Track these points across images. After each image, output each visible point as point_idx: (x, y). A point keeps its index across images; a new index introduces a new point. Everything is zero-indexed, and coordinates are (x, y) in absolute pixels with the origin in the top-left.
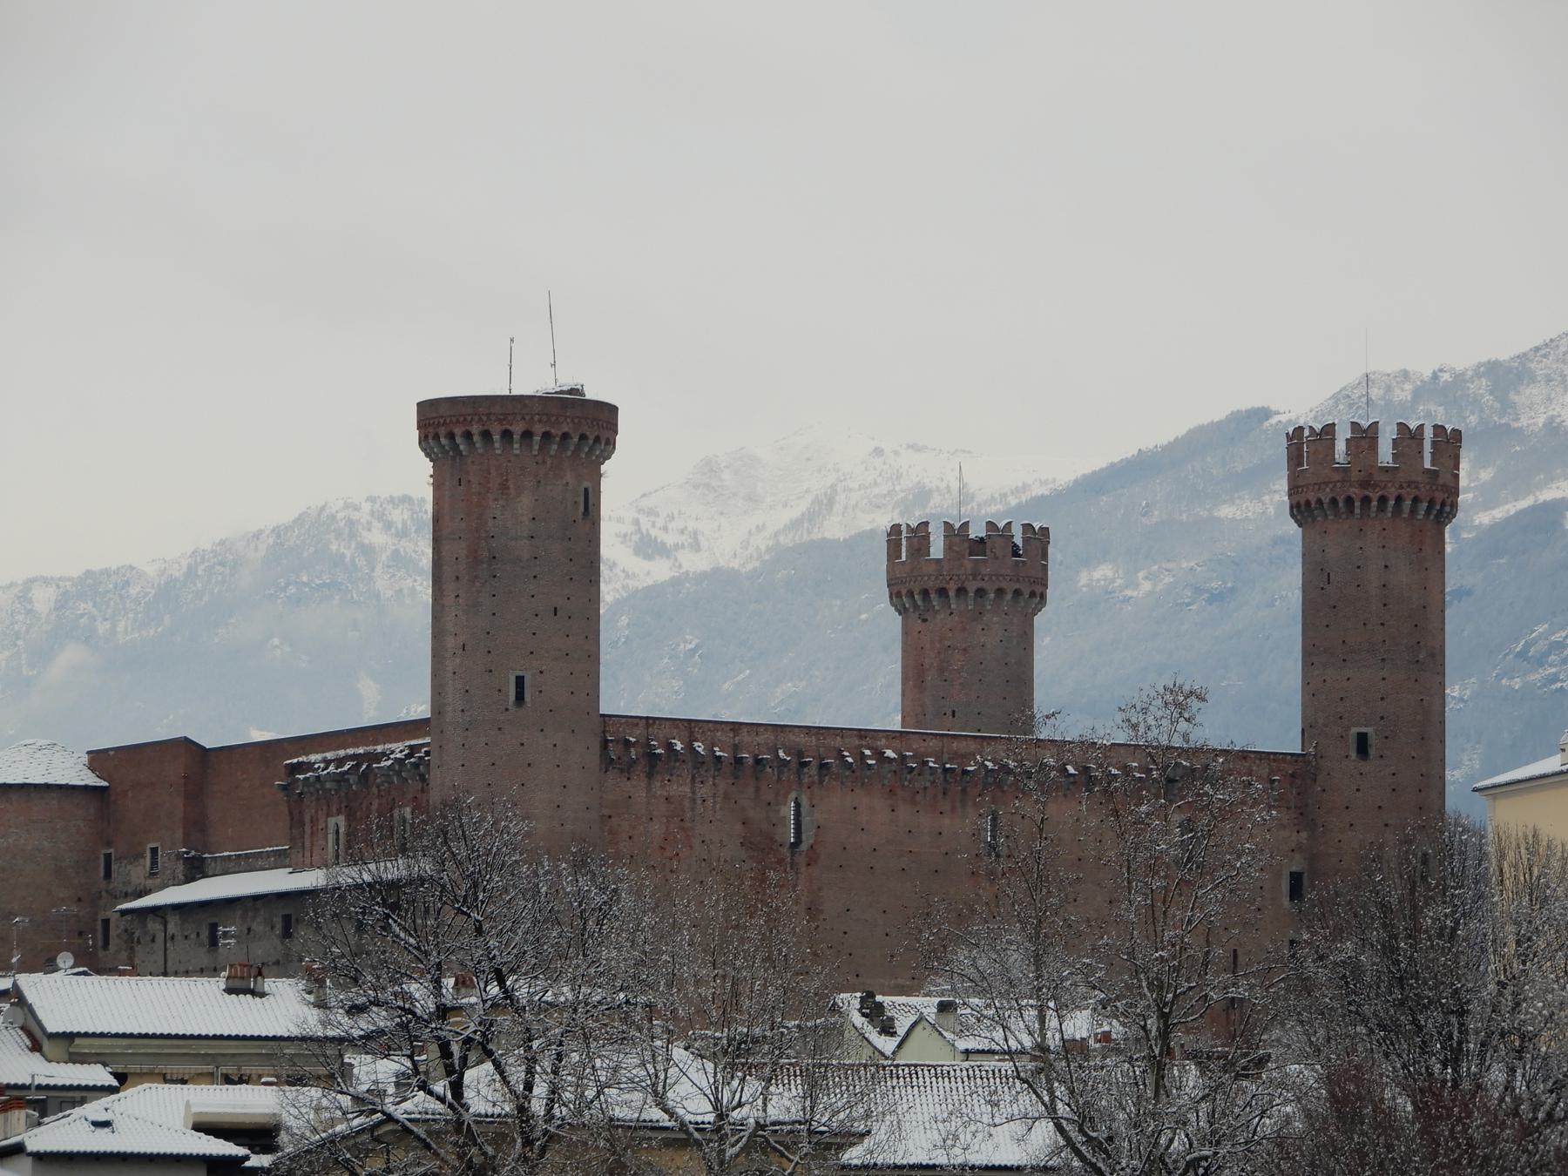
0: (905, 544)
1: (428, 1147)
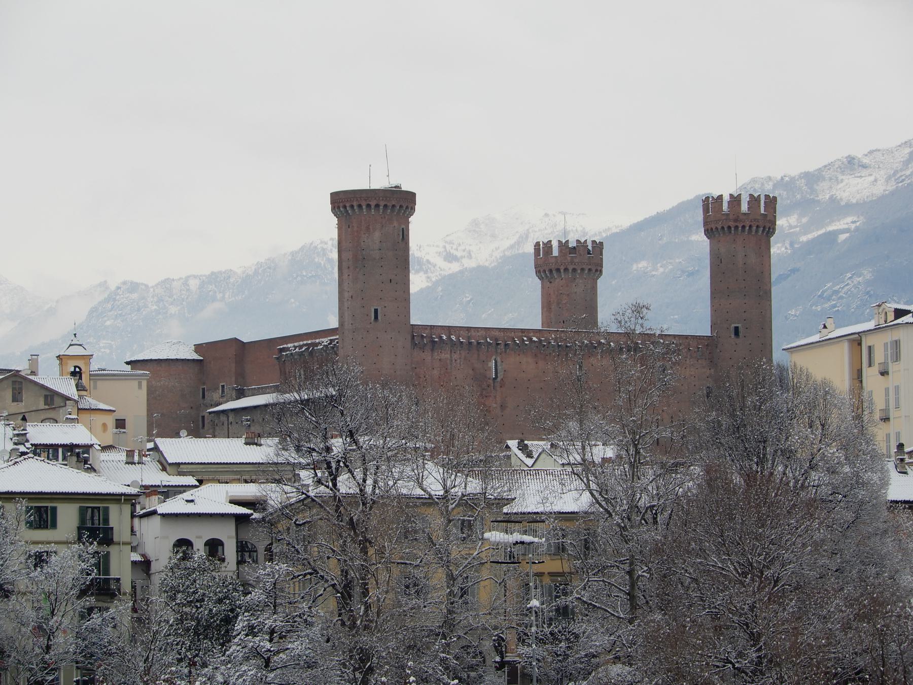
0: (542, 250)
1: (322, 507)
